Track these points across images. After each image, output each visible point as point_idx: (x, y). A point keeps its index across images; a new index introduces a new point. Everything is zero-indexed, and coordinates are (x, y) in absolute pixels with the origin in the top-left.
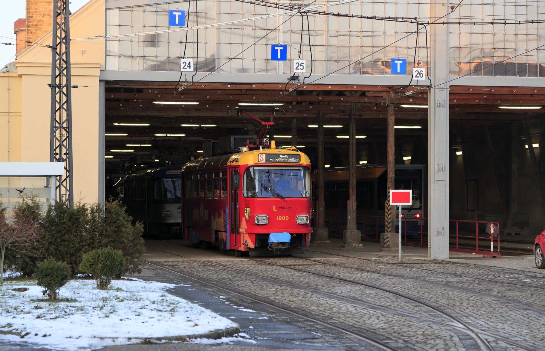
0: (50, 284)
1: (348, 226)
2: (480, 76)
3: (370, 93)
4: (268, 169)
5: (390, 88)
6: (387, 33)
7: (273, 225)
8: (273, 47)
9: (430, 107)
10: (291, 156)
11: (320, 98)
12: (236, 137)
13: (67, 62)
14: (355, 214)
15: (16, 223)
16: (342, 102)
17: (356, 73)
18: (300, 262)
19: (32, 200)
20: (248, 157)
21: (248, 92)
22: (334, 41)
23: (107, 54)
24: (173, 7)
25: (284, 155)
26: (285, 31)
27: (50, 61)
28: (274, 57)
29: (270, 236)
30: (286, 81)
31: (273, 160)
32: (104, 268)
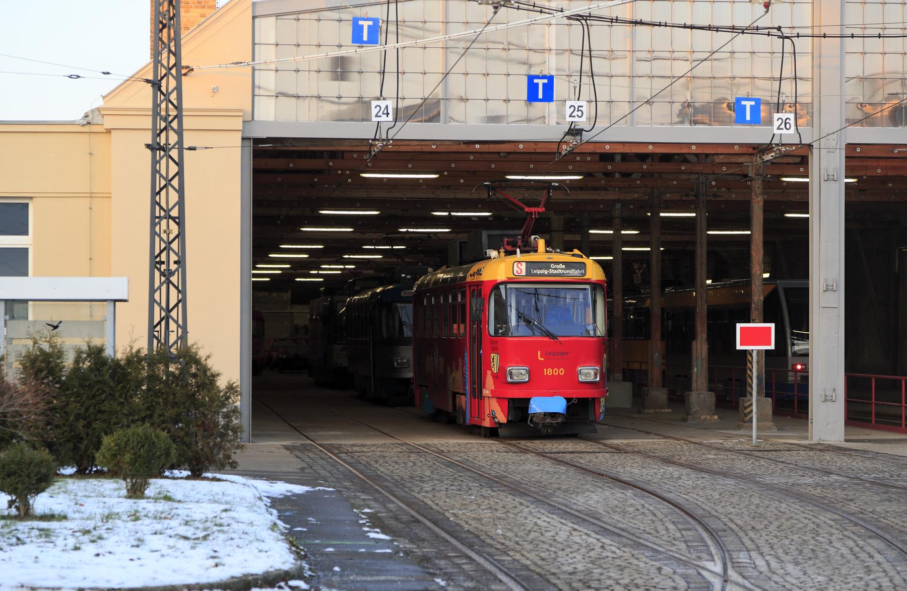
0: (16, 489)
1: (694, 385)
2: (900, 128)
3: (721, 157)
4: (533, 290)
5: (754, 148)
6: (736, 55)
7: (538, 383)
8: (531, 78)
9: (813, 180)
10: (569, 265)
11: (645, 167)
12: (491, 232)
13: (178, 108)
14: (705, 365)
15: (24, 382)
16: (683, 172)
17: (682, 122)
18: (581, 446)
19: (49, 342)
20: (500, 267)
21: (510, 156)
22: (643, 68)
23: (256, 93)
24: (358, 12)
25: (558, 263)
26: (560, 52)
27: (149, 105)
28: (532, 96)
29: (532, 402)
30: (558, 137)
31: (539, 272)
32: (136, 461)
